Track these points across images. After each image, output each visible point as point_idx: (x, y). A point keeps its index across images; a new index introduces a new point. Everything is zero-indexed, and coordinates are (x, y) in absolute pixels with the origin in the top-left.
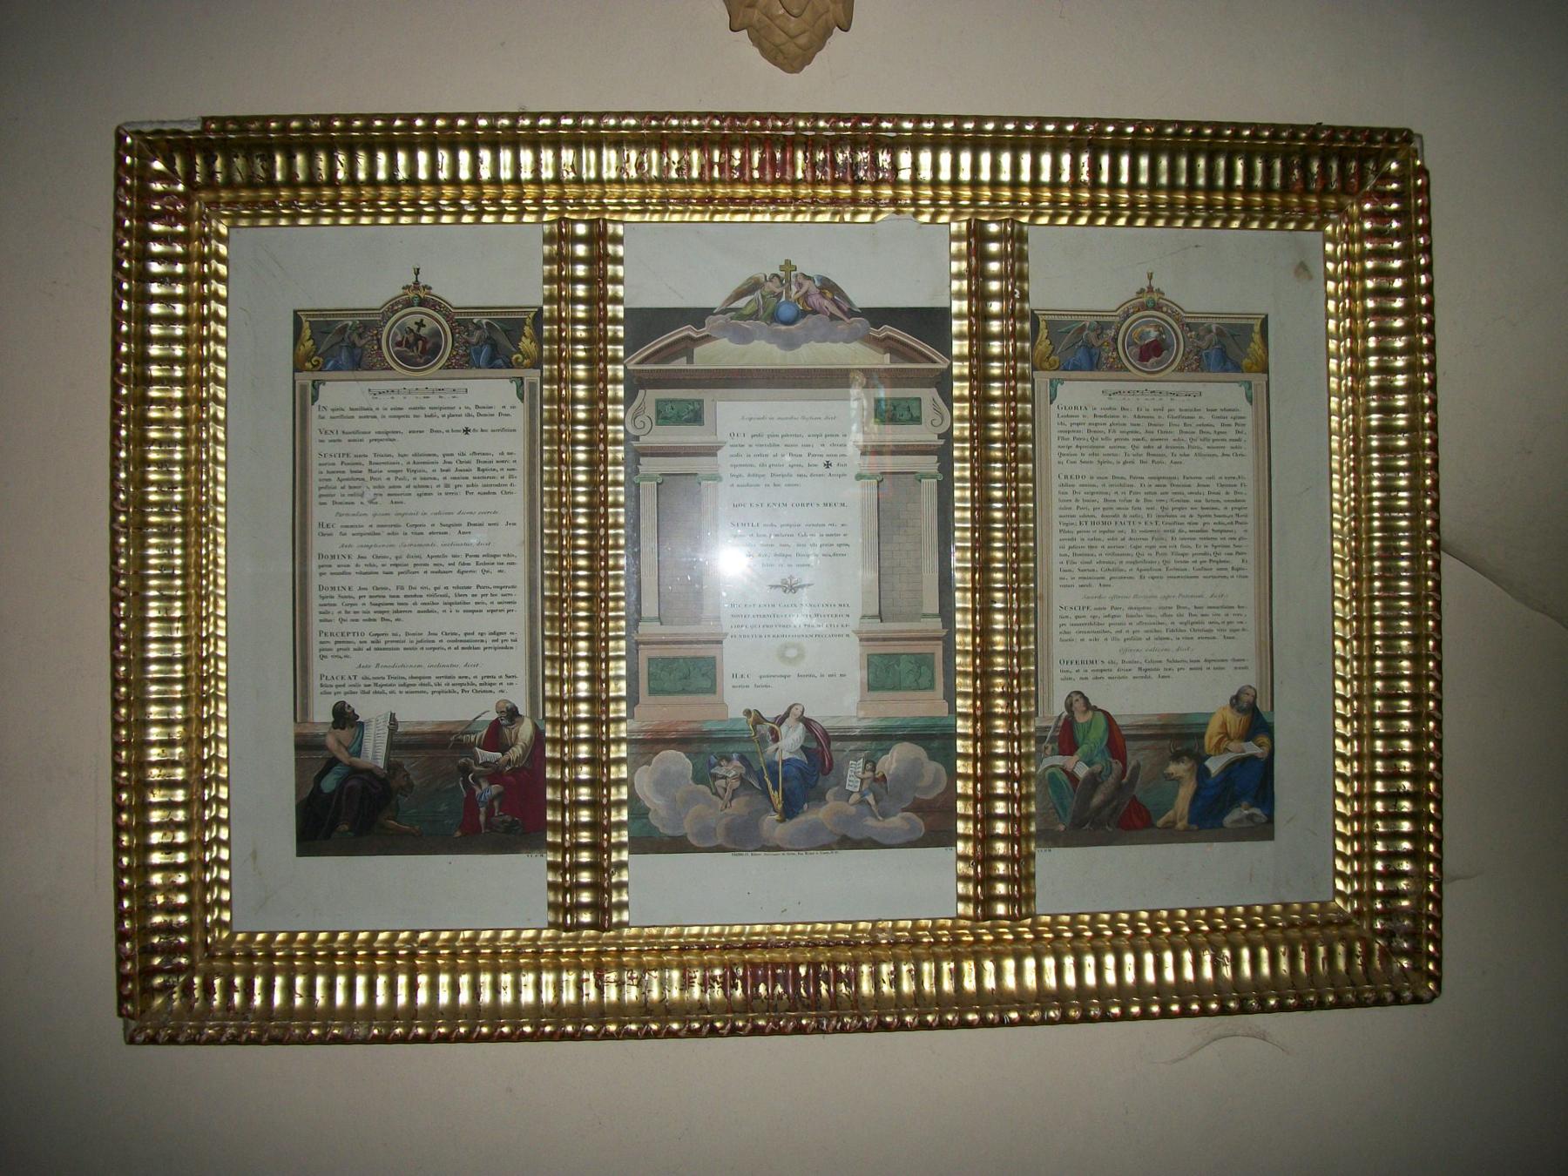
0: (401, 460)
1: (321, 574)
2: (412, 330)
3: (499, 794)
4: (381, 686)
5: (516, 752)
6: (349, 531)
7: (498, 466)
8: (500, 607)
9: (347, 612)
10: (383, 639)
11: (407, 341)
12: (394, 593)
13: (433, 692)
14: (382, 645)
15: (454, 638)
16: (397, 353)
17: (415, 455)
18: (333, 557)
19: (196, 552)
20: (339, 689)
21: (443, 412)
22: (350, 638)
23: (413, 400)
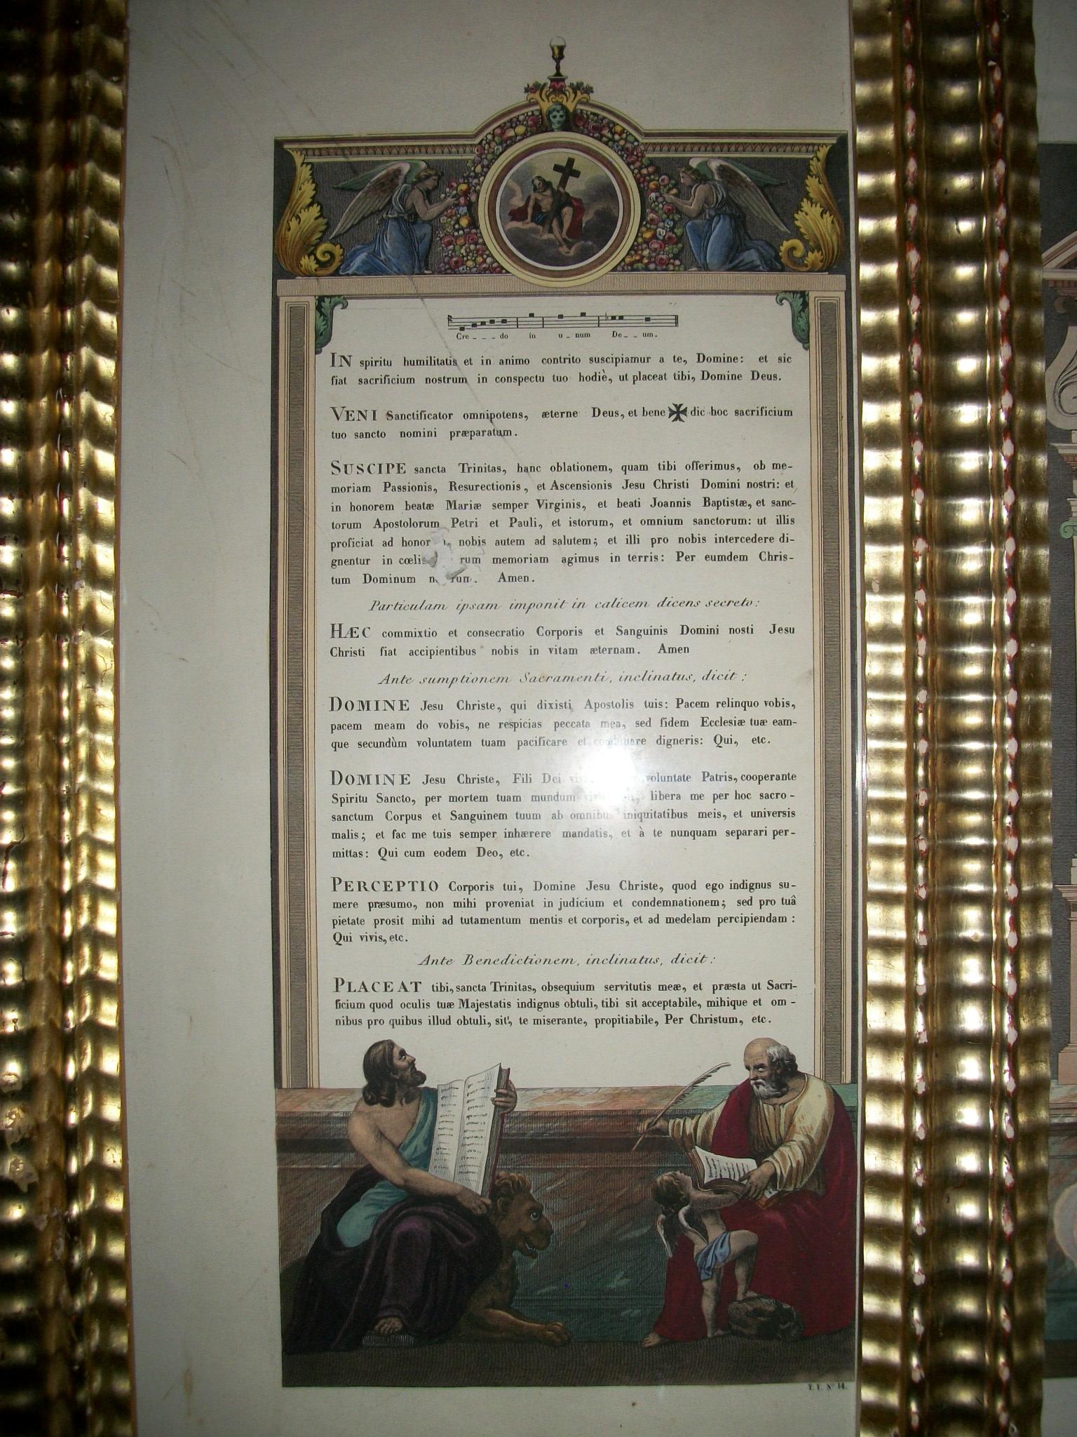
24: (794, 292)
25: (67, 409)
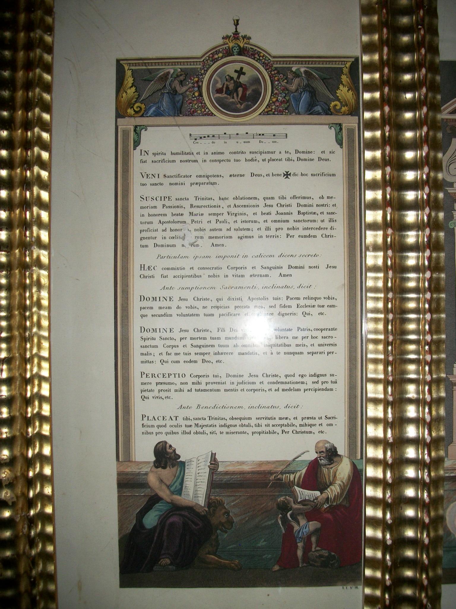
0: (221, 203)
1: (142, 316)
2: (232, 78)
3: (316, 531)
4: (202, 426)
5: (334, 490)
6: (171, 273)
7: (318, 210)
8: (321, 349)
9: (168, 354)
10: (203, 380)
11: (227, 88)
12: (215, 334)
13: (253, 433)
14: (203, 387)
15: (274, 379)
16: (217, 100)
17: (236, 198)
18: (155, 299)
19: (20, 295)
20: (161, 430)
21: (264, 156)
22: (172, 379)
23: (232, 145)
24: (336, 124)
25: (28, 173)
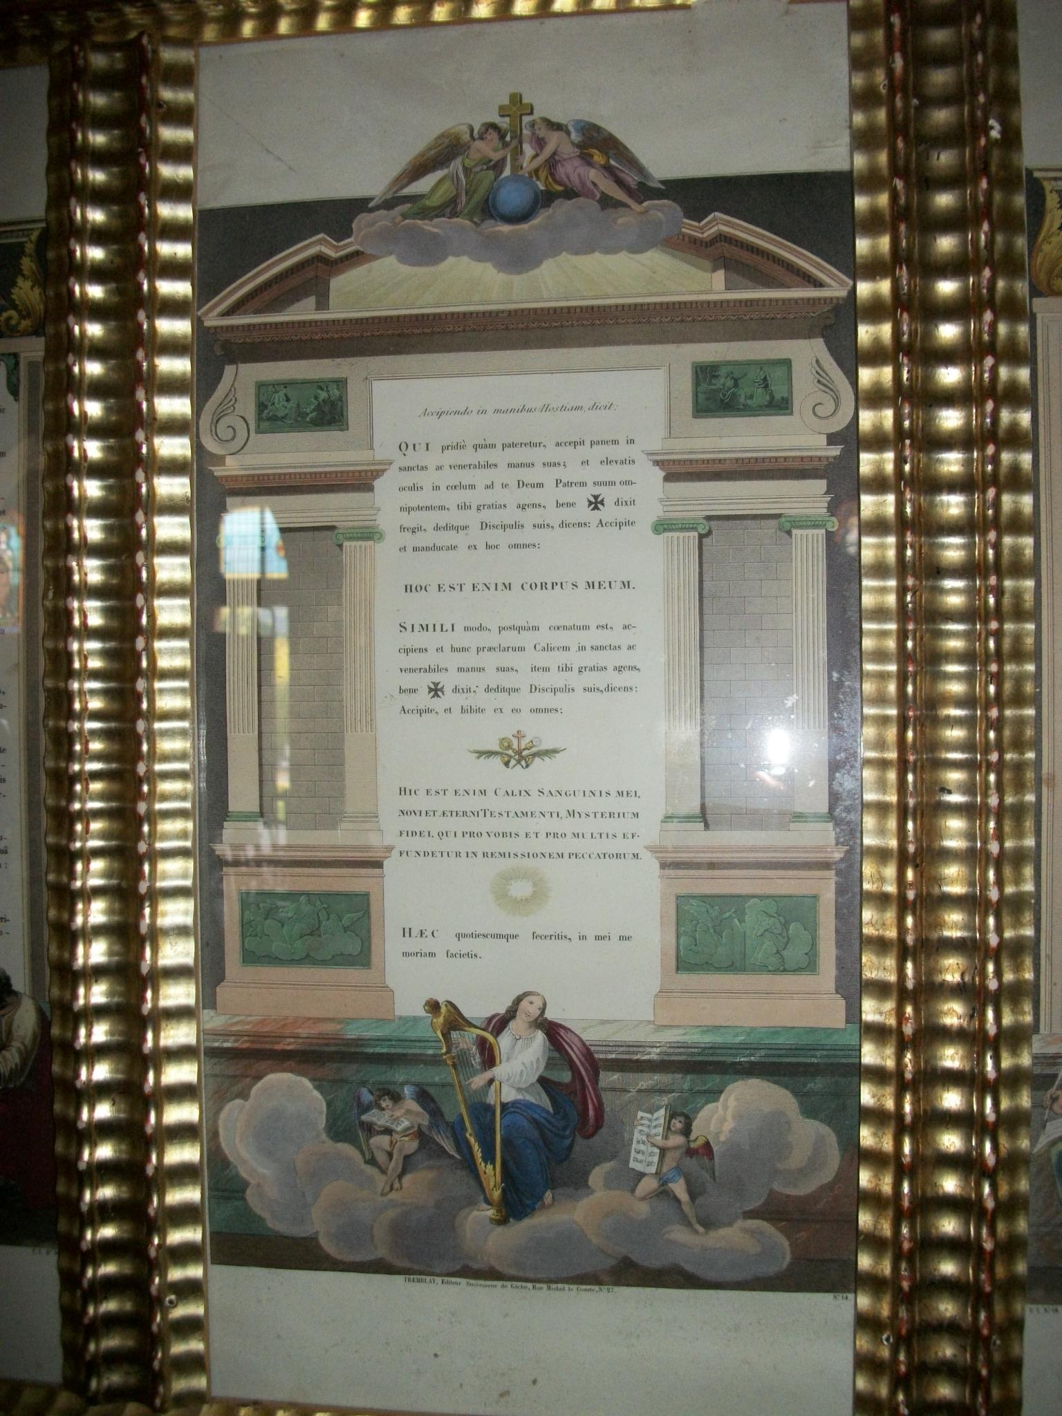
24: (9, 354)
